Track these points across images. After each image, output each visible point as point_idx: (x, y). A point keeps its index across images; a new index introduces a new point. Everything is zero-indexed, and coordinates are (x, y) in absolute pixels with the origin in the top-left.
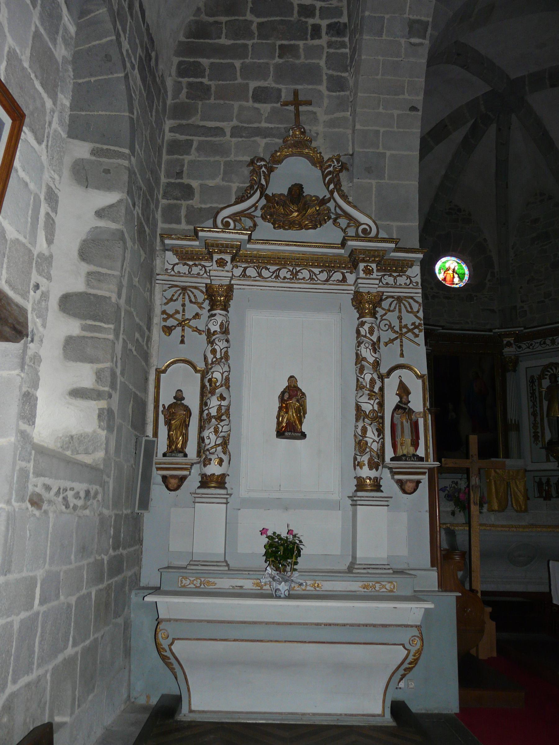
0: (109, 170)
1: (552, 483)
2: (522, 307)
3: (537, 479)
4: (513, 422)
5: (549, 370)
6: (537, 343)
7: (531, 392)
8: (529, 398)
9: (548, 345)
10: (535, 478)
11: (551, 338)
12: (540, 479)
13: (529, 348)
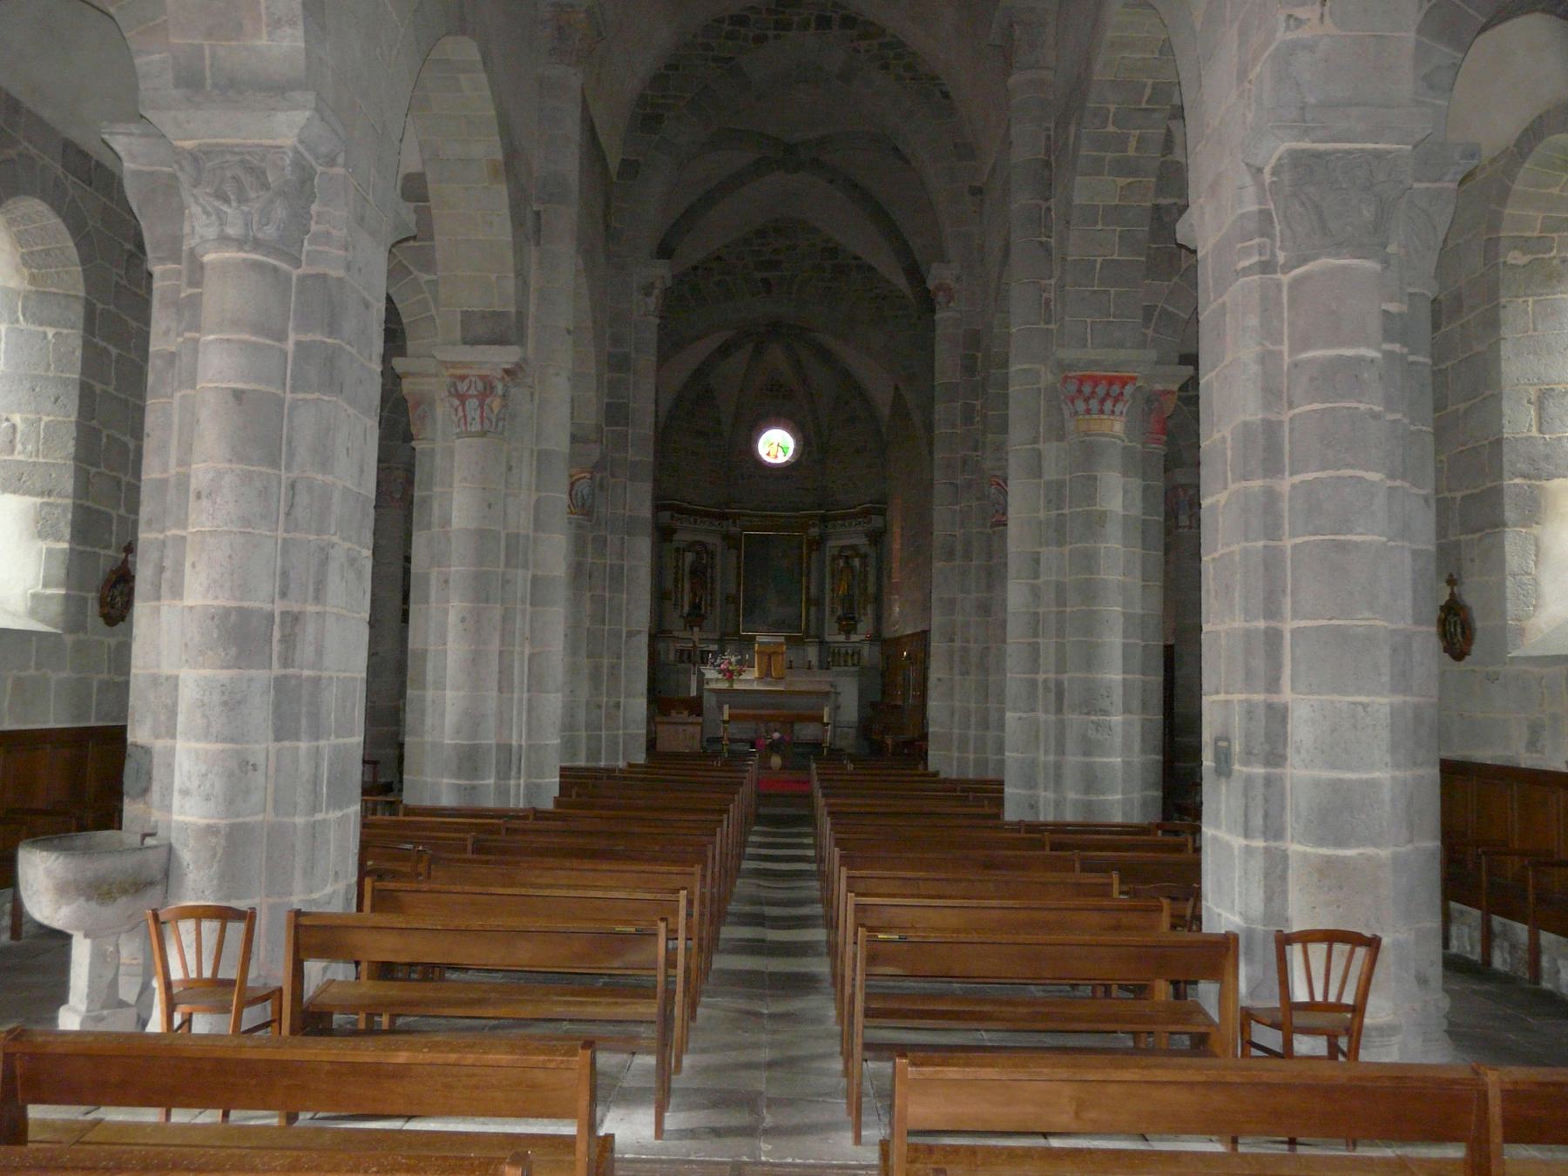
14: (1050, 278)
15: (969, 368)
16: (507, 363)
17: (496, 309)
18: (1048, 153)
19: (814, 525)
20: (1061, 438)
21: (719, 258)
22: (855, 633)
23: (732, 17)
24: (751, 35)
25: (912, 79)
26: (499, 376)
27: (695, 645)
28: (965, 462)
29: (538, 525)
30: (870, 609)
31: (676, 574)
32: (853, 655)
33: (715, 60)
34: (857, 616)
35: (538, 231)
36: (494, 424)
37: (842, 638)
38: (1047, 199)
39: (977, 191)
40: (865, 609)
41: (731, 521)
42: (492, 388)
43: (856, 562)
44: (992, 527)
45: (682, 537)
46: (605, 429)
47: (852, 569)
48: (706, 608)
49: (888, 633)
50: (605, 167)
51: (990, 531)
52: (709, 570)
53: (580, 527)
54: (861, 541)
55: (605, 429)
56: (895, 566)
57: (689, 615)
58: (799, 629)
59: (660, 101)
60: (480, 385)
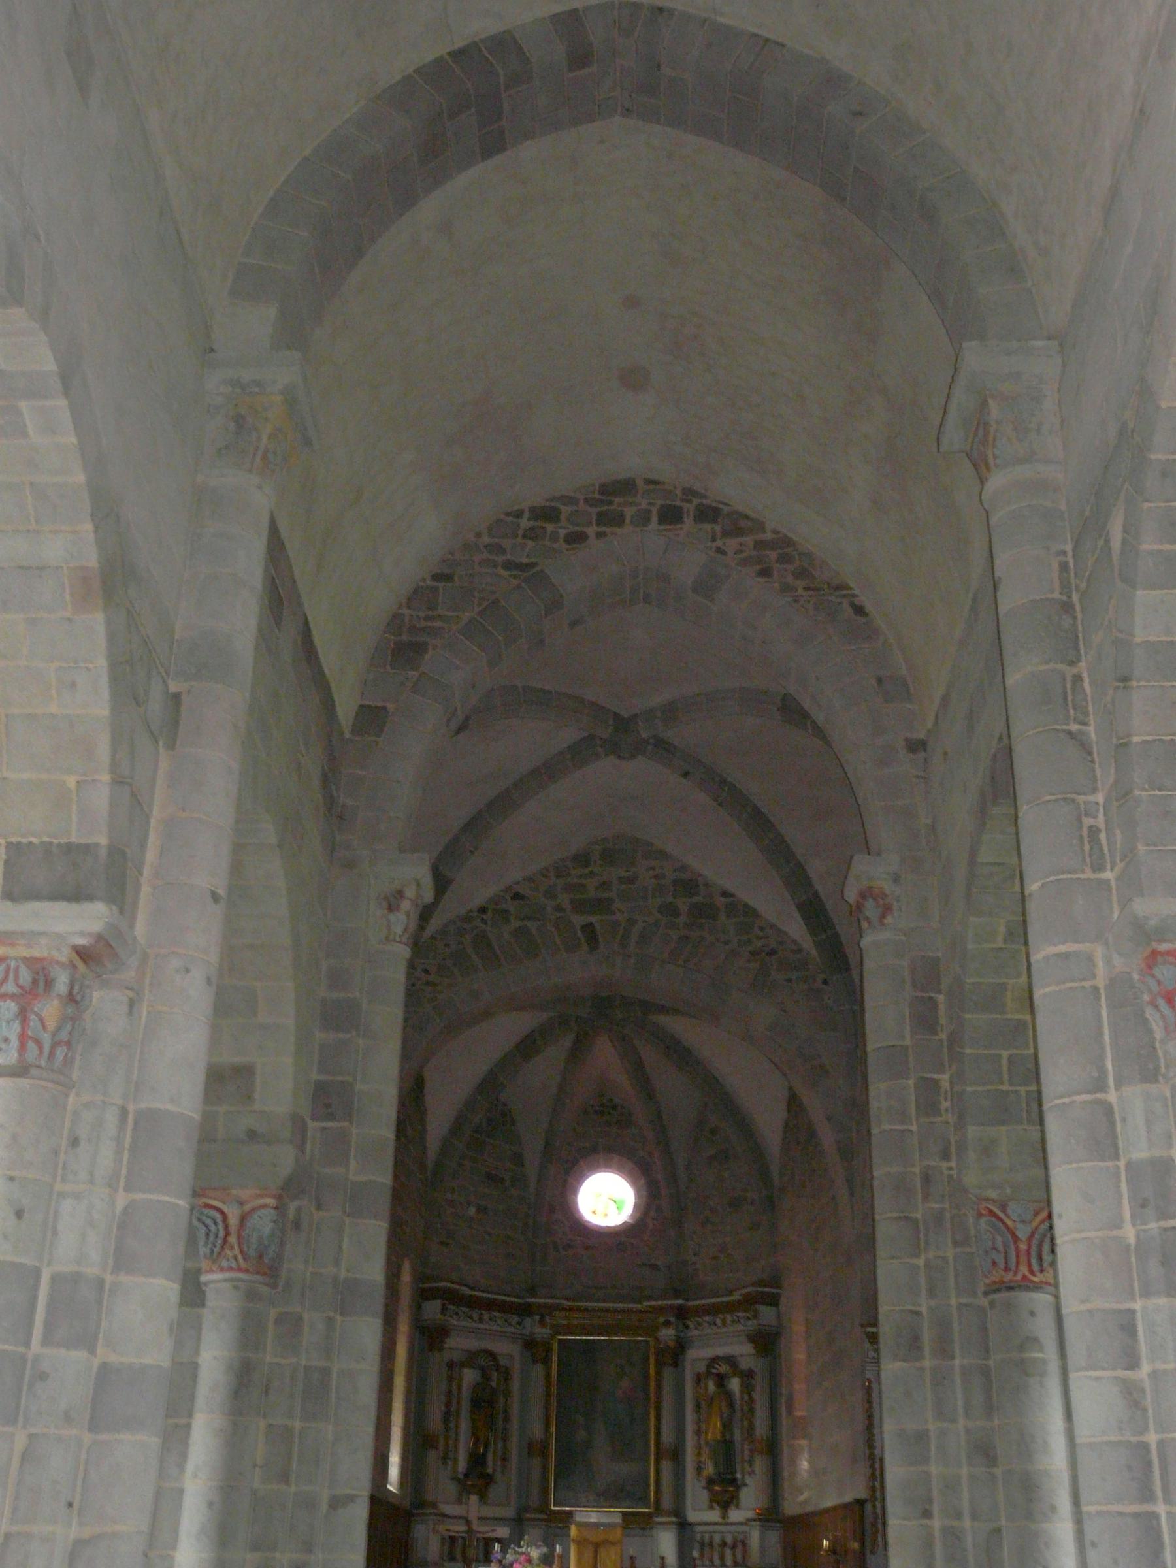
14: (1094, 790)
15: (925, 1020)
16: (82, 934)
17: (73, 839)
18: (1066, 587)
19: (667, 1324)
20: (1151, 1075)
21: (517, 896)
22: (737, 1506)
23: (533, 510)
24: (562, 533)
25: (807, 589)
26: (64, 960)
27: (470, 1531)
28: (927, 1179)
29: (122, 1260)
30: (760, 1465)
32: (734, 1547)
33: (508, 566)
34: (739, 1476)
35: (174, 723)
36: (46, 1049)
37: (714, 1515)
38: (1072, 663)
39: (916, 746)
40: (751, 1463)
42: (49, 983)
43: (735, 1384)
44: (986, 1294)
45: (458, 1344)
46: (312, 1125)
47: (729, 1396)
49: (792, 1506)
50: (329, 705)
51: (984, 1302)
52: (502, 1401)
53: (251, 1295)
54: (744, 1351)
55: (312, 1125)
56: (799, 1387)
57: (466, 1475)
58: (644, 1500)
59: (423, 624)
60: (25, 976)
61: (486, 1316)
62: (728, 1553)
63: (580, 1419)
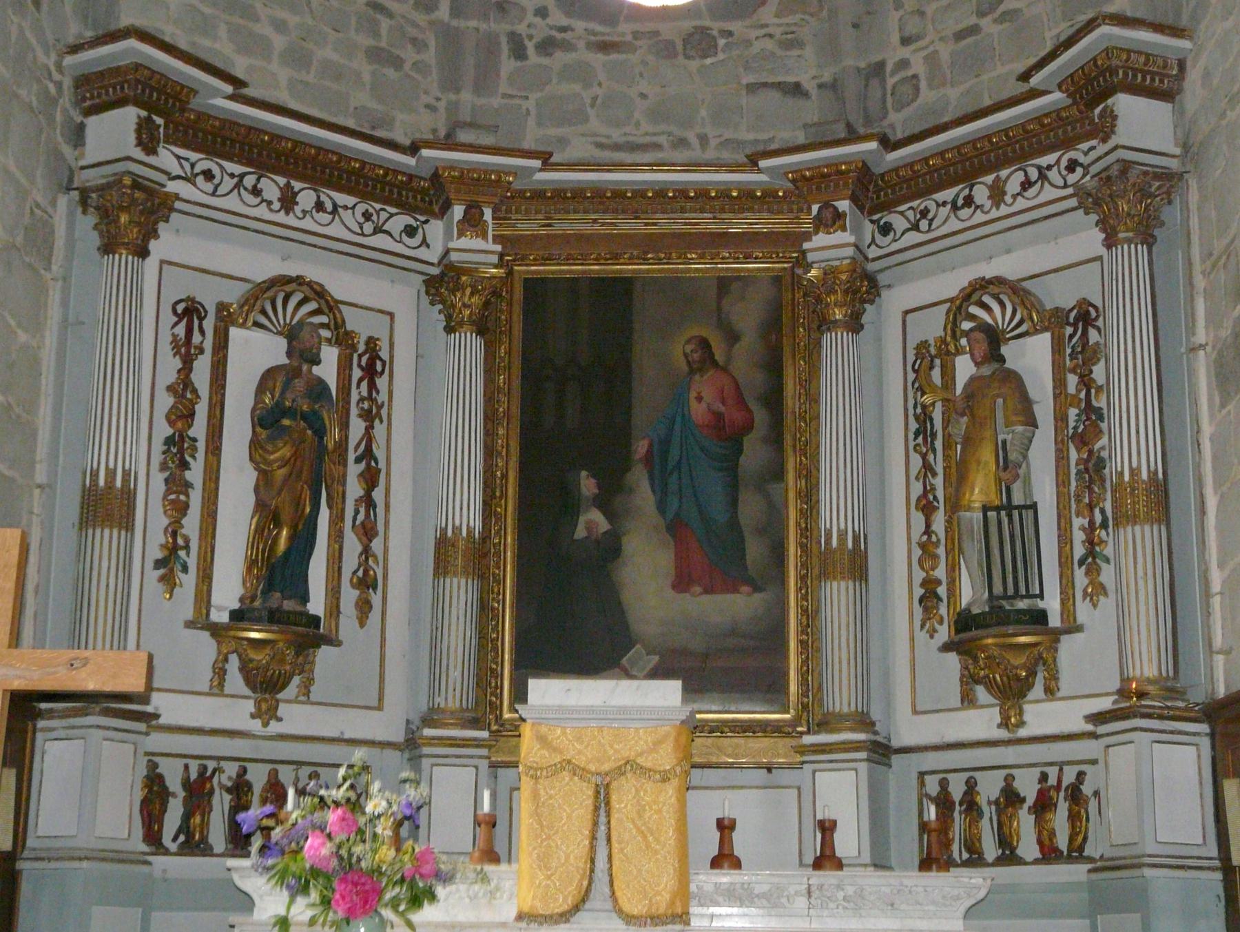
0: (545, 8)
1: (982, 800)
2: (904, 64)
3: (932, 786)
4: (102, 482)
5: (974, 310)
6: (944, 204)
7: (919, 410)
8: (911, 436)
9: (269, 203)
10: (927, 777)
11: (989, 179)
12: (944, 784)
13: (915, 227)
31: (182, 415)
32: (1043, 805)
34: (1052, 604)
41: (458, 211)
48: (334, 593)
61: (306, 199)
62: (1025, 822)
63: (587, 485)
